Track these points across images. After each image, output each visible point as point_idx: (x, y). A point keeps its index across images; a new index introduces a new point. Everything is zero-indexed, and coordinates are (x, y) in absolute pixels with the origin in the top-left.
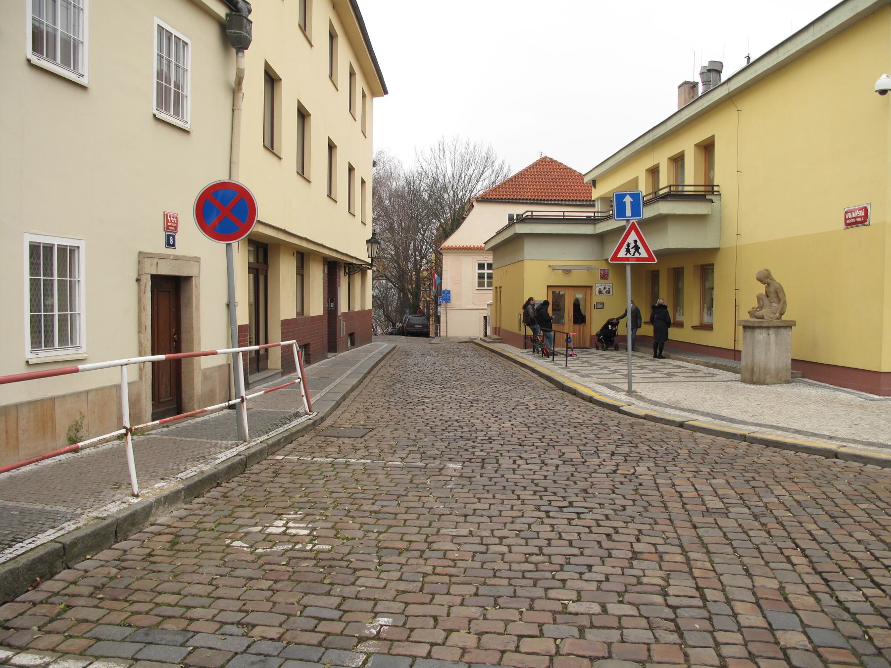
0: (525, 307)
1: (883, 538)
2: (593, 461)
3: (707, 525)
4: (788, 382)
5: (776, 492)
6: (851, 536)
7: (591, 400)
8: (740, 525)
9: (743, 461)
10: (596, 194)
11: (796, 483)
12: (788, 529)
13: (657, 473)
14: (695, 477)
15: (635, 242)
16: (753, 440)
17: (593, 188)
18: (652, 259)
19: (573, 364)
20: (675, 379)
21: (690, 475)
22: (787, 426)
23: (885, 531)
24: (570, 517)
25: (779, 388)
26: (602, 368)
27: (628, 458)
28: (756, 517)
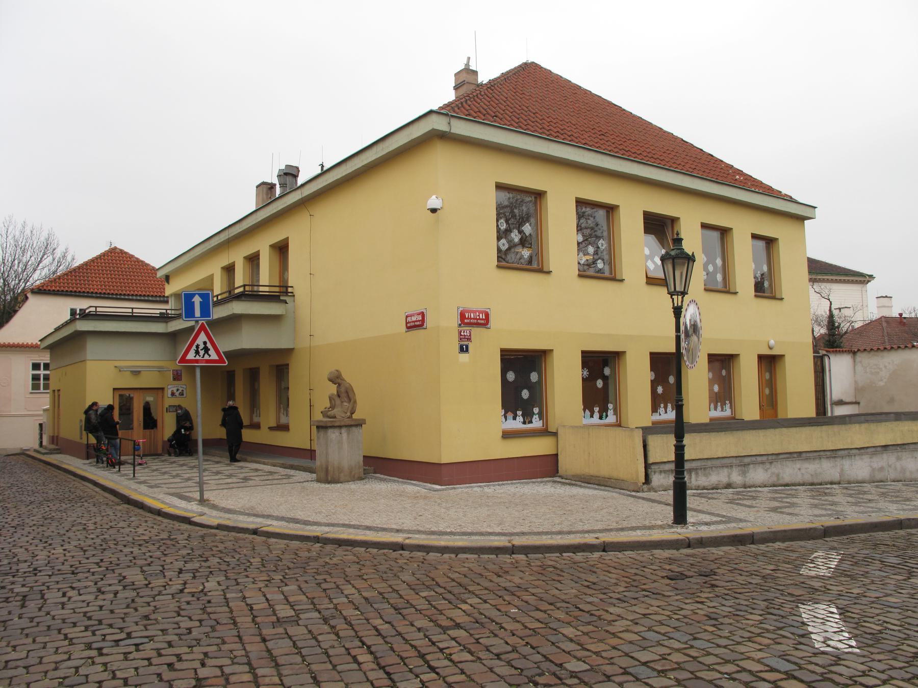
0: (86, 412)
1: (439, 622)
2: (158, 582)
3: (277, 636)
4: (361, 479)
5: (346, 592)
6: (412, 625)
7: (159, 513)
8: (310, 632)
9: (316, 563)
10: (170, 290)
11: (365, 580)
12: (356, 628)
13: (227, 587)
14: (267, 586)
15: (205, 343)
16: (325, 541)
17: (166, 284)
18: (223, 361)
19: (142, 474)
20: (251, 483)
21: (261, 585)
22: (358, 523)
23: (442, 616)
24: (127, 651)
25: (353, 486)
26: (174, 477)
27: (197, 574)
28: (325, 620)
